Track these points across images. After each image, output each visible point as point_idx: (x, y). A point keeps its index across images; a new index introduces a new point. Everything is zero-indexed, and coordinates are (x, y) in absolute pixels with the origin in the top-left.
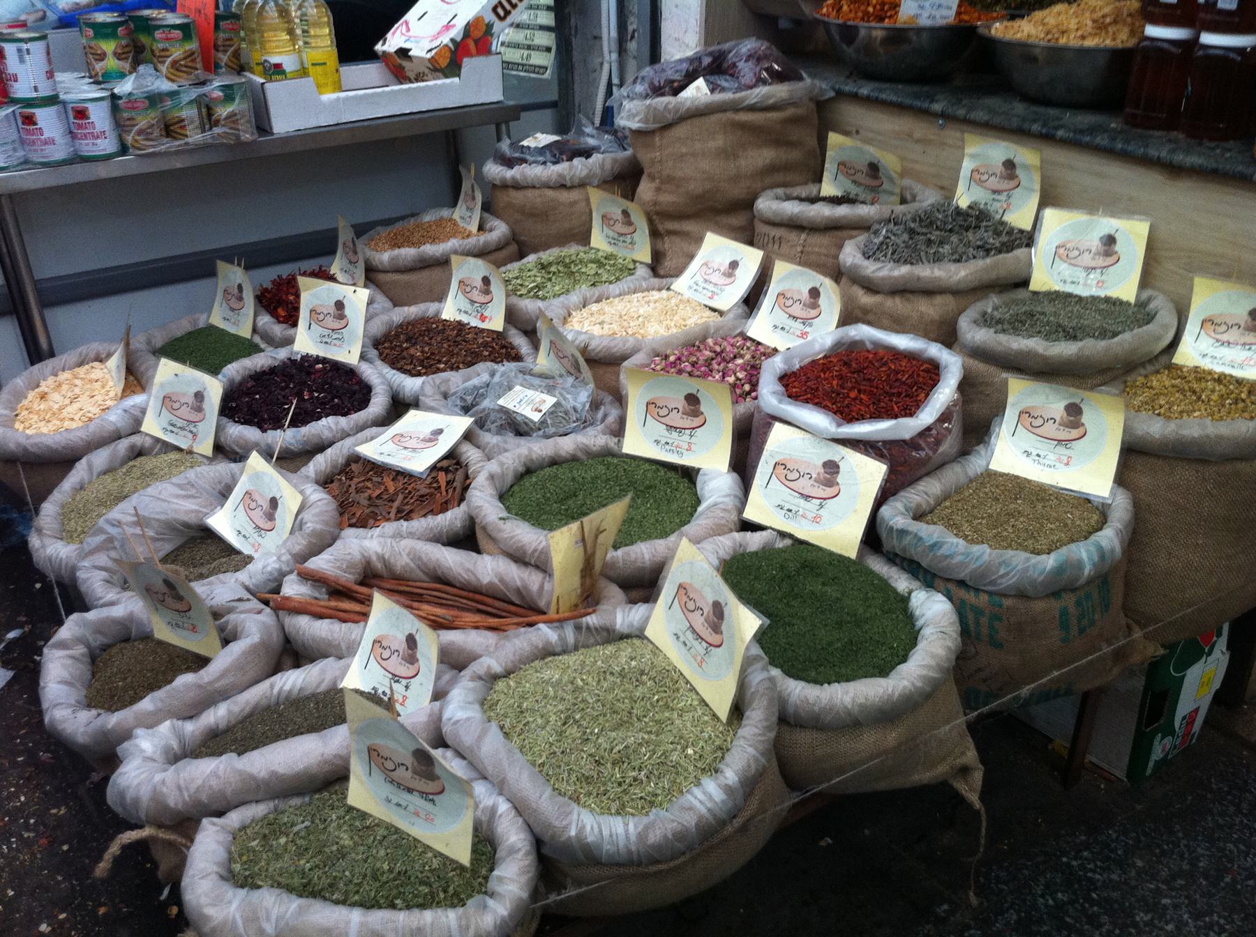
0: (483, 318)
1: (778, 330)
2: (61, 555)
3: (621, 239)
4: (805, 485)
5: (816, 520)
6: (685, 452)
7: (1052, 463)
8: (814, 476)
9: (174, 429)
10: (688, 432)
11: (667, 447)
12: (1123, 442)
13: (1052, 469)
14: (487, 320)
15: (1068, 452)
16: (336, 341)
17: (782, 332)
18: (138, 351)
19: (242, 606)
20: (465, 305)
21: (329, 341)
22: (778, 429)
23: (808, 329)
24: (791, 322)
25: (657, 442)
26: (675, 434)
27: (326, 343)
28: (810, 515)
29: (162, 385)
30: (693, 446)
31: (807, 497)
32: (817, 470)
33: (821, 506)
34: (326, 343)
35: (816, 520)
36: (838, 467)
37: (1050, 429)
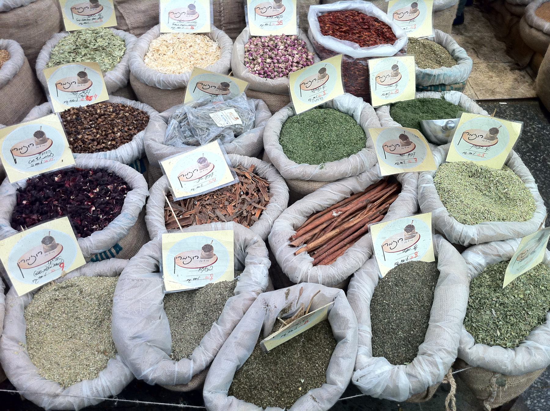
0: (89, 98)
1: (265, 27)
2: (104, 384)
3: (91, 18)
4: (389, 81)
5: (397, 92)
6: (323, 96)
7: (410, 30)
8: (390, 75)
9: (40, 275)
10: (322, 87)
11: (315, 99)
12: (433, 10)
13: (411, 32)
14: (93, 98)
15: (414, 23)
16: (45, 159)
17: (266, 27)
18: (301, 213)
19: (291, 297)
20: (69, 96)
21: (39, 162)
22: (371, 63)
23: (281, 19)
24: (269, 20)
25: (310, 100)
26: (316, 91)
27: (37, 164)
28: (394, 92)
29: (10, 259)
30: (326, 92)
31: (390, 85)
32: (390, 71)
33: (397, 85)
34: (37, 164)
35: (397, 92)
36: (397, 66)
37: (407, 17)
